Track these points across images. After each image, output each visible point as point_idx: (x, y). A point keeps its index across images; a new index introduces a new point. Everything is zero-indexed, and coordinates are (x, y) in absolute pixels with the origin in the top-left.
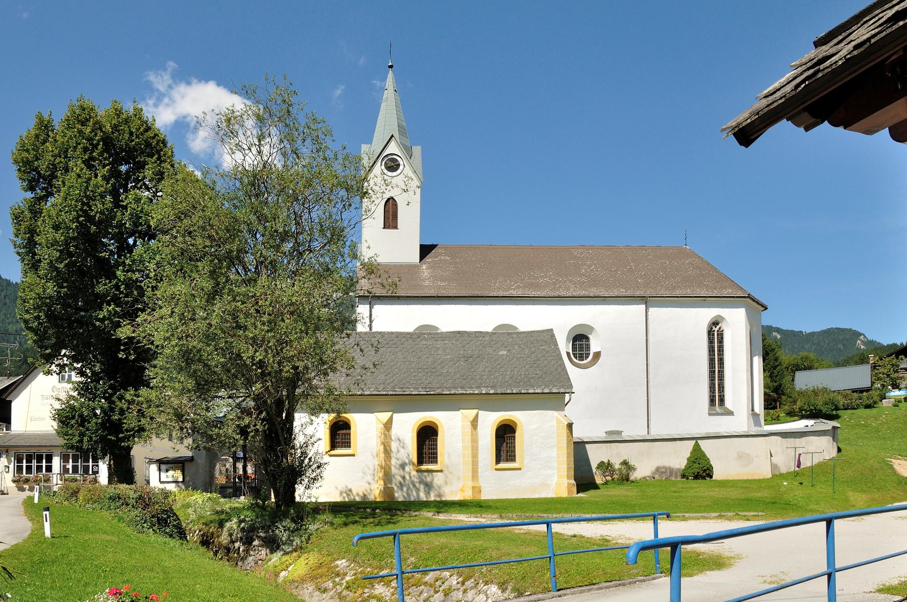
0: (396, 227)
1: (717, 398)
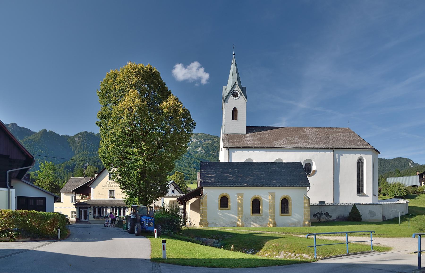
0: (237, 120)
1: (360, 191)
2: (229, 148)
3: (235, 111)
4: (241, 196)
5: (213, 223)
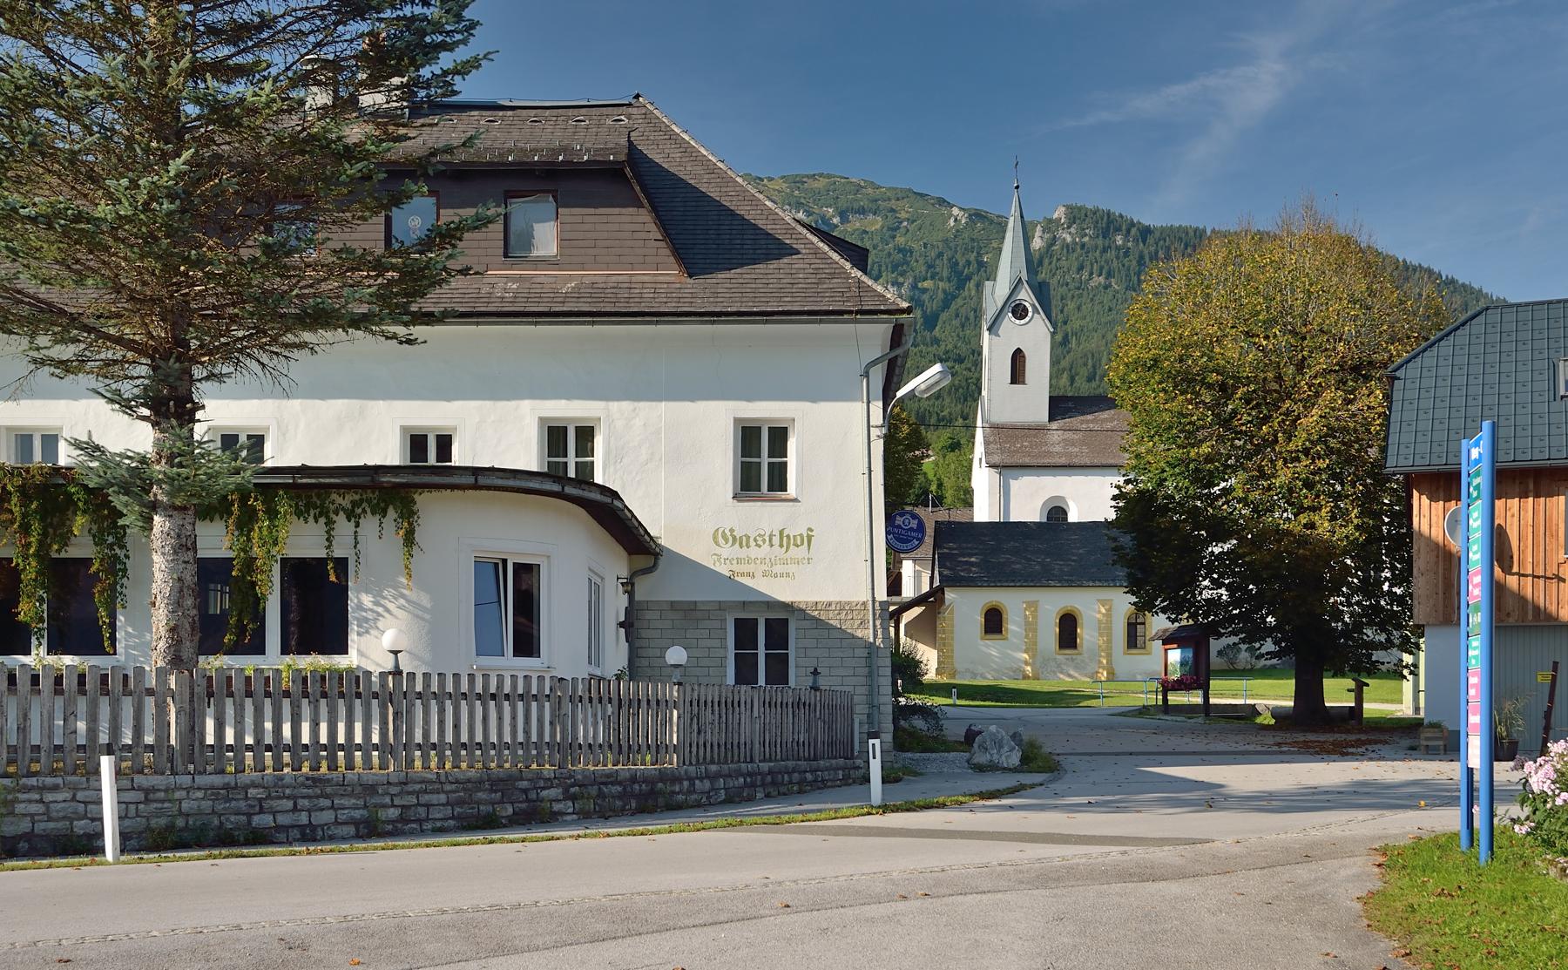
2: (1005, 468)
3: (1018, 358)
4: (1033, 609)
5: (967, 670)
